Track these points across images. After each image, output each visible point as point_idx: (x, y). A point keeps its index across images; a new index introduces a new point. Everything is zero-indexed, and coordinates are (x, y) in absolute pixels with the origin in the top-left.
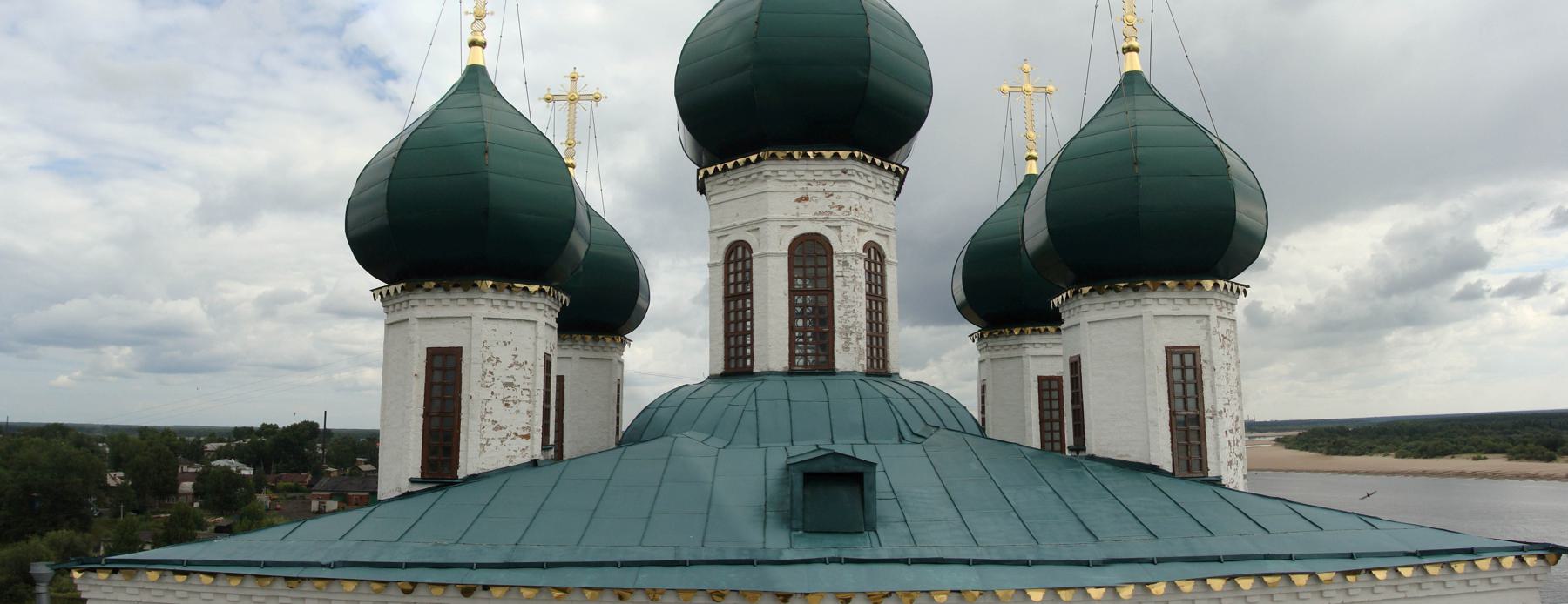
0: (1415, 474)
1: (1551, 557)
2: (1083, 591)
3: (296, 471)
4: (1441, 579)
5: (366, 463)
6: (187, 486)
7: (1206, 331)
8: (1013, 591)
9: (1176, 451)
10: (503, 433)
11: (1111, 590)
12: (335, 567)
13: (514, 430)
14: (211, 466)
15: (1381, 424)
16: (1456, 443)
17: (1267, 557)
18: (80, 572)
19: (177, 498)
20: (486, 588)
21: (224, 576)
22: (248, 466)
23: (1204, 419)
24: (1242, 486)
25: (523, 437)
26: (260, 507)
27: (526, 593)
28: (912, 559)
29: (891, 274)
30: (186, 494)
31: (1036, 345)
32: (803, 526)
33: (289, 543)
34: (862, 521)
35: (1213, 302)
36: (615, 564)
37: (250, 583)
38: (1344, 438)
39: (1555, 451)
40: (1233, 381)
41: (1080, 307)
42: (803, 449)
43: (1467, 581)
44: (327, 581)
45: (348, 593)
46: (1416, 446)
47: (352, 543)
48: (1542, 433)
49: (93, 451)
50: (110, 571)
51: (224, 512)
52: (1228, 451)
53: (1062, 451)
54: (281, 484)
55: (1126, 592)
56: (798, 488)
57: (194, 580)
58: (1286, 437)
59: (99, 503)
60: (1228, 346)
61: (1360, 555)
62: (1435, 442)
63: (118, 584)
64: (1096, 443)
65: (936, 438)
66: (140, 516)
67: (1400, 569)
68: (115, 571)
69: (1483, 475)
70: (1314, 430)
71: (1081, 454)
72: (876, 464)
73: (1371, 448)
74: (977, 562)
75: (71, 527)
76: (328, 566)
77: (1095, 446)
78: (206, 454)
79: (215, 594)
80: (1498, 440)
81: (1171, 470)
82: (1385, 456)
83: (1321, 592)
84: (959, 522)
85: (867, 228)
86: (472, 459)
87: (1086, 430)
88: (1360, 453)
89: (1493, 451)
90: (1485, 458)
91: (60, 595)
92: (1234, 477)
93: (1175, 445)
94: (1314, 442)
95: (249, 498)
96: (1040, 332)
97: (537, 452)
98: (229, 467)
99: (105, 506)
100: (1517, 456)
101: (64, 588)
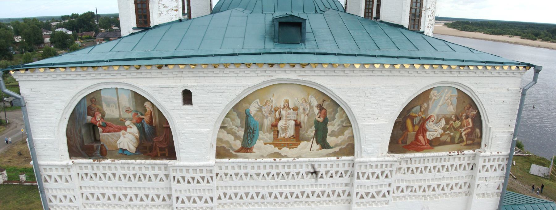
0: (489, 40)
1: (528, 68)
2: (373, 65)
3: (88, 31)
4: (491, 71)
5: (115, 26)
6: (47, 40)
8: (350, 64)
10: (167, 9)
11: (382, 65)
12: (110, 61)
13: (171, 8)
14: (55, 31)
15: (481, 22)
16: (505, 31)
17: (435, 59)
18: (13, 71)
19: (44, 44)
20: (166, 65)
21: (69, 68)
22: (70, 30)
23: (422, 10)
24: (431, 35)
25: (175, 10)
26: (77, 46)
27: (181, 66)
28: (317, 53)
30: (48, 43)
32: (279, 41)
33: (91, 54)
34: (302, 40)
36: (212, 56)
37: (79, 70)
38: (467, 25)
39: (537, 37)
42: (279, 14)
43: (499, 73)
44: (108, 67)
45: (116, 70)
46: (491, 31)
47: (115, 52)
48: (534, 30)
49: (6, 29)
50: (25, 70)
51: (64, 49)
52: (428, 22)
53: (371, 19)
54: (84, 36)
55: (387, 66)
56: (277, 27)
57: (58, 70)
58: (448, 23)
59: (14, 49)
61: (466, 61)
62: (498, 30)
63: (29, 74)
64: (383, 17)
65: (328, 12)
66: (31, 53)
67: (478, 67)
68: (27, 70)
69: (511, 43)
70: (458, 21)
71: (378, 20)
72: (306, 20)
73: (476, 30)
74: (339, 54)
75: (5, 59)
76: (107, 61)
77: (383, 17)
78: (52, 27)
79: (67, 75)
80: (519, 31)
81: (407, 28)
82: (480, 33)
83: (451, 72)
84: (334, 41)
86: (155, 20)
87: (380, 12)
88: (472, 31)
89: (517, 35)
90: (513, 37)
91: (8, 84)
92: (429, 32)
95: (72, 43)
97: (181, 17)
98: (63, 31)
99: (17, 50)
100: (524, 37)
101: (8, 82)
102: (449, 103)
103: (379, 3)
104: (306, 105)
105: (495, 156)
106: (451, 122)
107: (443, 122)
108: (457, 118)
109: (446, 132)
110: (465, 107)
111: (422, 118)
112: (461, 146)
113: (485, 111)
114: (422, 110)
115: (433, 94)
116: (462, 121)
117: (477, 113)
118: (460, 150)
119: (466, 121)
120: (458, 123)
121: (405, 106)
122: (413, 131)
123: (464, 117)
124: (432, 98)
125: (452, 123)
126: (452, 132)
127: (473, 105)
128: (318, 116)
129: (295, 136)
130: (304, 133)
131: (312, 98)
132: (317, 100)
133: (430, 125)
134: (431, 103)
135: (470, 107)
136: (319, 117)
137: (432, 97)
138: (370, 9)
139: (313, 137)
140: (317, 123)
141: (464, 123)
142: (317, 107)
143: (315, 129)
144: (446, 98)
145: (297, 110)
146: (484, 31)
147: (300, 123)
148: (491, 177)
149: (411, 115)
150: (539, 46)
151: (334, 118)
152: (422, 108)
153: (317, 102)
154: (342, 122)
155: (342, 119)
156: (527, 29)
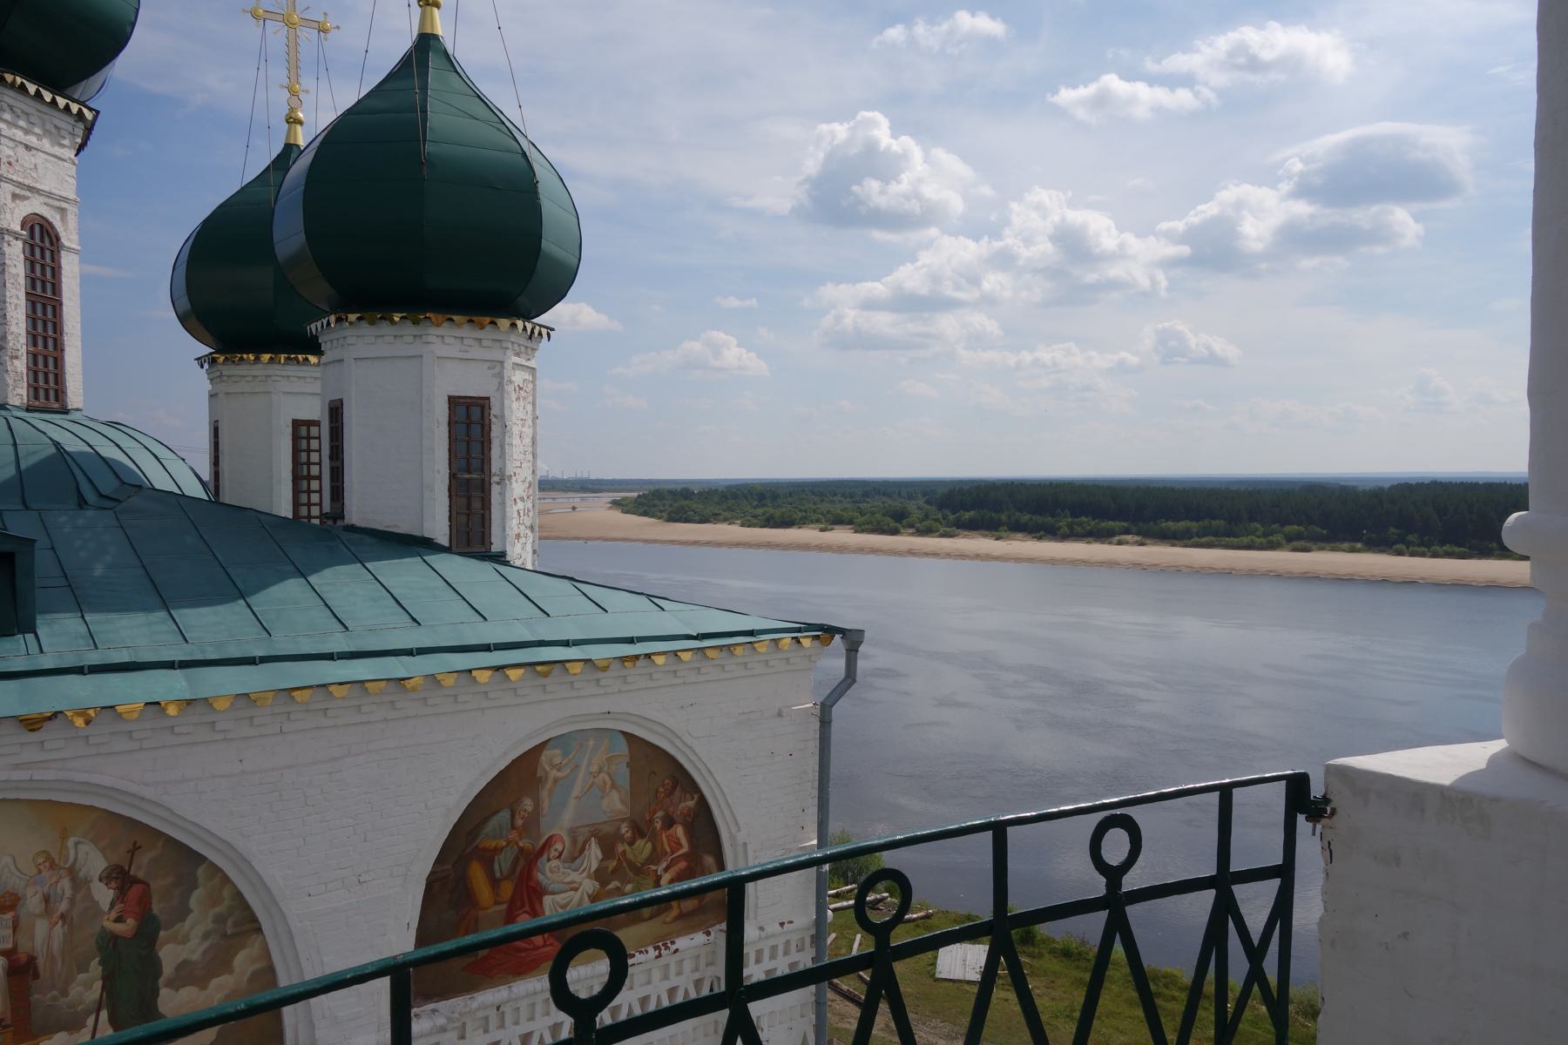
7: (499, 380)
9: (454, 521)
15: (729, 487)
16: (806, 511)
29: (70, 267)
31: (292, 379)
35: (510, 345)
39: (901, 523)
40: (528, 441)
41: (345, 338)
48: (890, 502)
58: (624, 499)
60: (525, 398)
67: (679, 654)
70: (657, 491)
71: (339, 523)
73: (717, 515)
83: (598, 680)
85: (28, 194)
89: (838, 521)
90: (832, 529)
93: (454, 514)
94: (655, 506)
96: (298, 362)
102: (605, 783)
103: (338, 464)
104: (54, 879)
105: (773, 936)
106: (620, 848)
107: (594, 854)
108: (639, 831)
109: (609, 884)
110: (657, 791)
111: (521, 850)
112: (665, 923)
113: (722, 791)
114: (519, 822)
115: (553, 766)
116: (654, 838)
117: (697, 803)
118: (662, 938)
119: (667, 837)
120: (643, 848)
121: (456, 820)
122: (497, 903)
123: (658, 825)
124: (546, 778)
125: (624, 852)
126: (629, 882)
127: (682, 779)
128: (113, 915)
129: (9, 1022)
130: (54, 998)
131: (80, 846)
132: (103, 851)
133: (551, 872)
134: (544, 794)
135: (674, 788)
136: (119, 920)
137: (547, 773)
138: (315, 478)
139: (96, 1006)
140: (110, 945)
141: (663, 844)
142: (106, 878)
143: (103, 971)
144: (594, 768)
145: (12, 907)
146: (741, 517)
147: (32, 959)
148: (773, 1012)
149: (481, 846)
150: (911, 553)
151: (183, 912)
152: (517, 817)
153: (103, 860)
154: (220, 919)
155: (218, 910)
156: (868, 499)
